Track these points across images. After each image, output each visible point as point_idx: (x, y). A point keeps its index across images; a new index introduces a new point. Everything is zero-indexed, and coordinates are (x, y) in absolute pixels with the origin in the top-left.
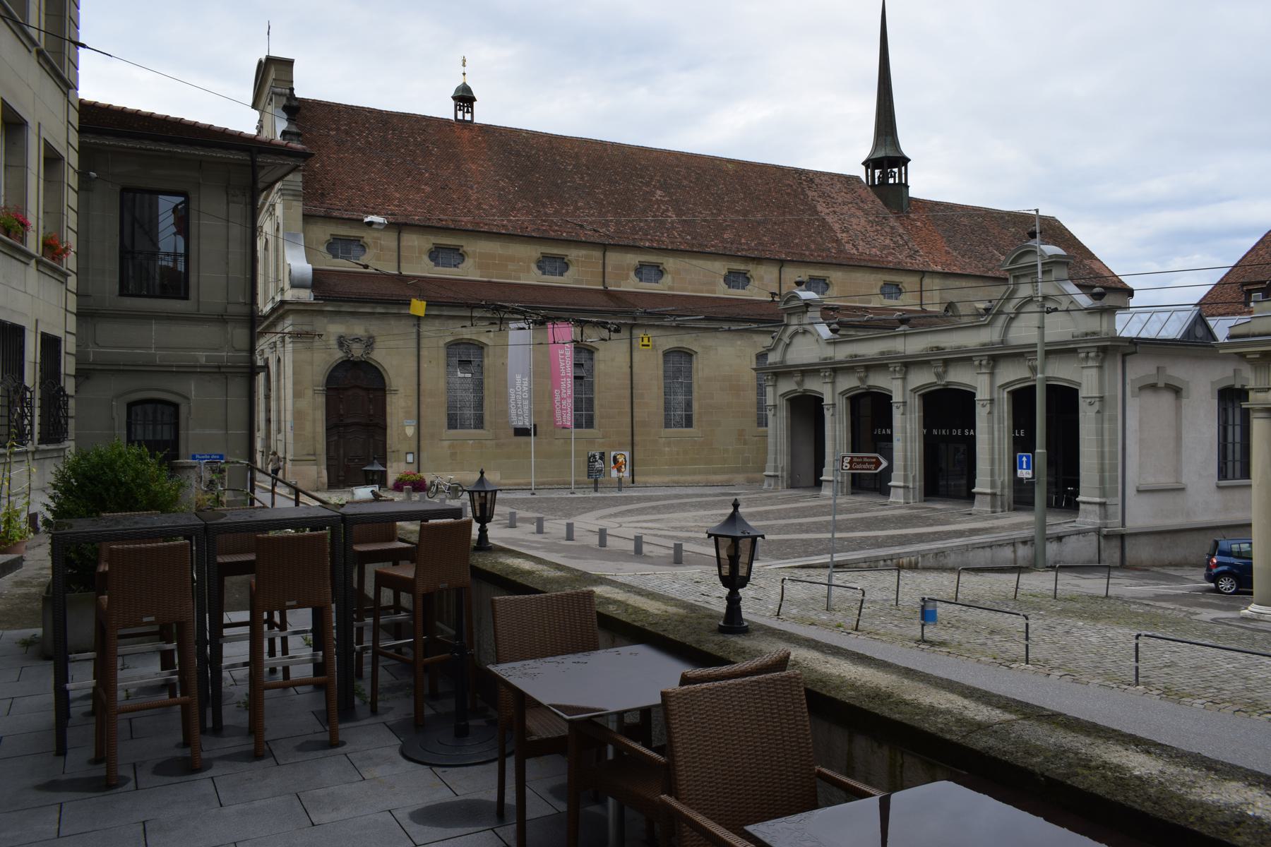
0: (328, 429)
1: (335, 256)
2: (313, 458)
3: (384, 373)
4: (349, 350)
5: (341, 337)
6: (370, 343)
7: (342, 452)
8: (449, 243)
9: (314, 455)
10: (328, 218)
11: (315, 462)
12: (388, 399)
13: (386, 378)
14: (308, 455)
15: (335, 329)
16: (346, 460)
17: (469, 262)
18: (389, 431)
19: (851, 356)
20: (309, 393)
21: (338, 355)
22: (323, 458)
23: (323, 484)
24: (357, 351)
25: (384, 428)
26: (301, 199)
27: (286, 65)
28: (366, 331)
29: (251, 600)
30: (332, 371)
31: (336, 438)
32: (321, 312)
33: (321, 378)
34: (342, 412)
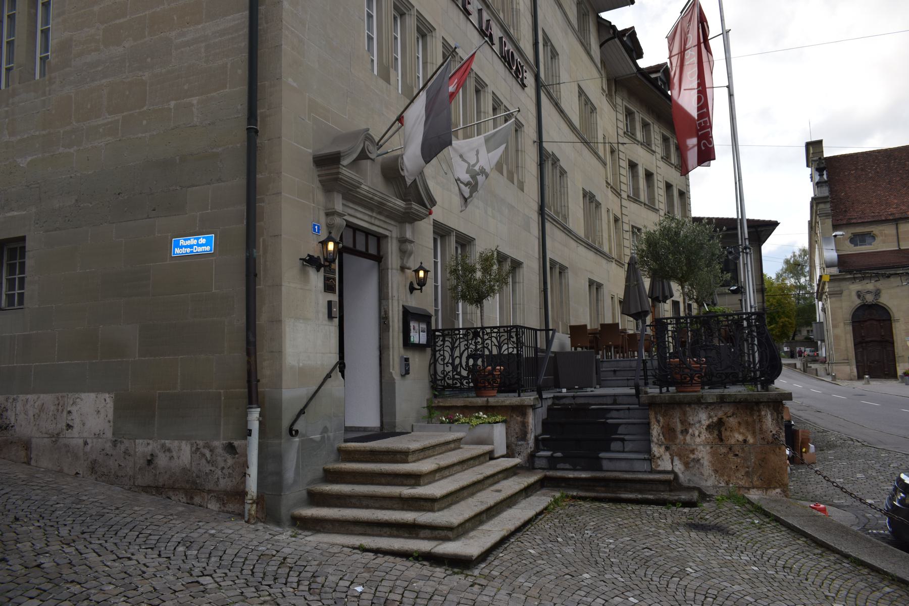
0: (855, 345)
1: (856, 245)
2: (847, 361)
3: (888, 310)
4: (864, 298)
5: (858, 292)
6: (877, 293)
7: (865, 358)
8: (858, 231)
9: (848, 360)
10: (849, 224)
11: (848, 364)
12: (893, 325)
13: (891, 313)
14: (844, 360)
15: (855, 287)
16: (869, 363)
17: (878, 240)
18: (895, 344)
19: (330, 316)
20: (842, 325)
21: (858, 302)
22: (854, 361)
23: (855, 376)
24: (870, 298)
25: (893, 343)
26: (831, 217)
27: (819, 143)
28: (875, 286)
29: (502, 406)
30: (855, 311)
31: (861, 350)
32: (845, 279)
33: (848, 316)
34: (863, 334)
